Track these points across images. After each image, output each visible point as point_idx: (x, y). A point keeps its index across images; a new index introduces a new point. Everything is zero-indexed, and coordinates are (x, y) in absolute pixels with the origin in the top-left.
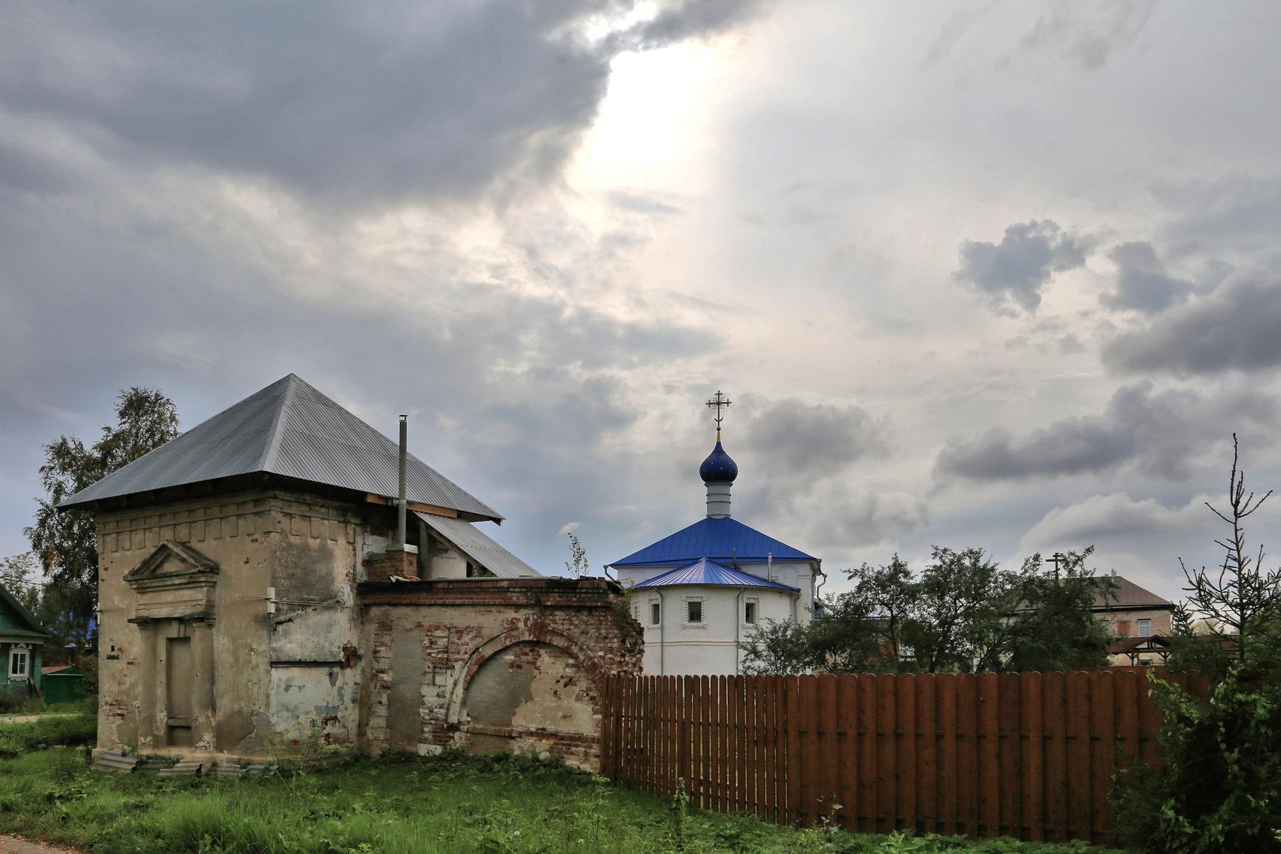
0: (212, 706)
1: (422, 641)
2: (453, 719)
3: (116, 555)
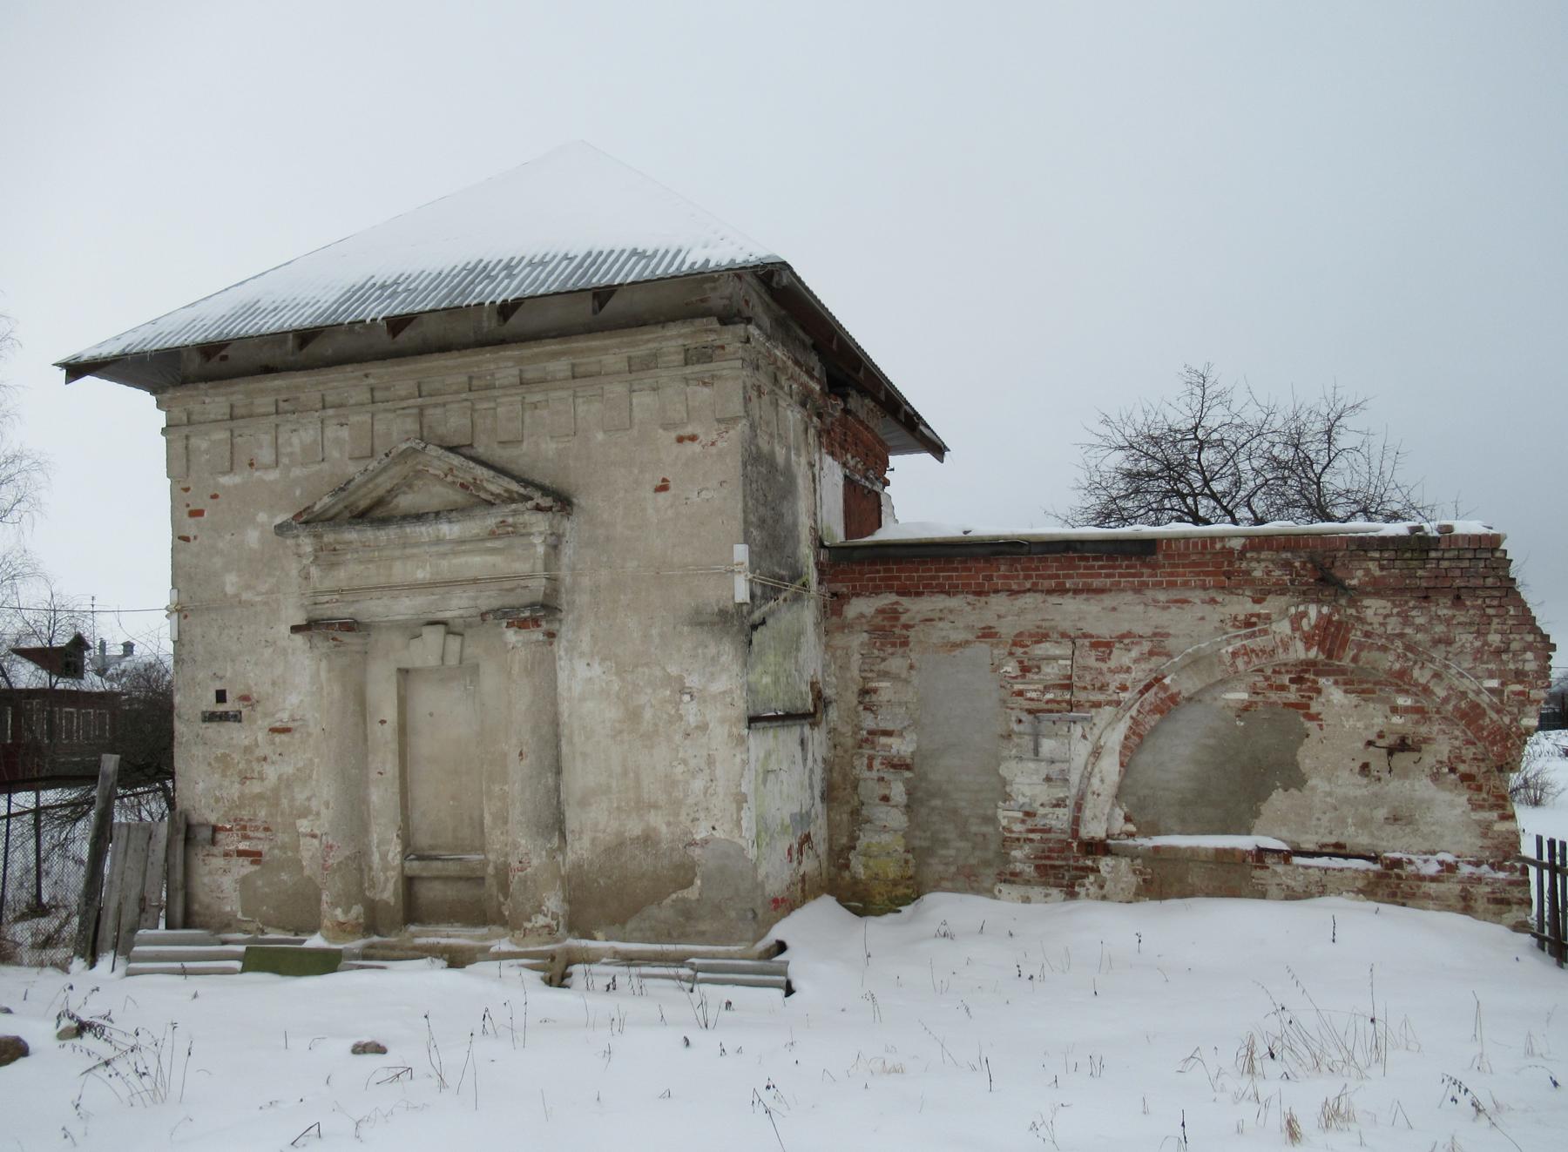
0: (555, 825)
1: (996, 668)
2: (1094, 829)
3: (225, 480)
